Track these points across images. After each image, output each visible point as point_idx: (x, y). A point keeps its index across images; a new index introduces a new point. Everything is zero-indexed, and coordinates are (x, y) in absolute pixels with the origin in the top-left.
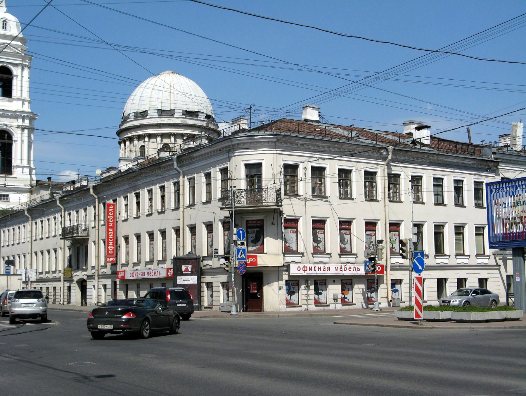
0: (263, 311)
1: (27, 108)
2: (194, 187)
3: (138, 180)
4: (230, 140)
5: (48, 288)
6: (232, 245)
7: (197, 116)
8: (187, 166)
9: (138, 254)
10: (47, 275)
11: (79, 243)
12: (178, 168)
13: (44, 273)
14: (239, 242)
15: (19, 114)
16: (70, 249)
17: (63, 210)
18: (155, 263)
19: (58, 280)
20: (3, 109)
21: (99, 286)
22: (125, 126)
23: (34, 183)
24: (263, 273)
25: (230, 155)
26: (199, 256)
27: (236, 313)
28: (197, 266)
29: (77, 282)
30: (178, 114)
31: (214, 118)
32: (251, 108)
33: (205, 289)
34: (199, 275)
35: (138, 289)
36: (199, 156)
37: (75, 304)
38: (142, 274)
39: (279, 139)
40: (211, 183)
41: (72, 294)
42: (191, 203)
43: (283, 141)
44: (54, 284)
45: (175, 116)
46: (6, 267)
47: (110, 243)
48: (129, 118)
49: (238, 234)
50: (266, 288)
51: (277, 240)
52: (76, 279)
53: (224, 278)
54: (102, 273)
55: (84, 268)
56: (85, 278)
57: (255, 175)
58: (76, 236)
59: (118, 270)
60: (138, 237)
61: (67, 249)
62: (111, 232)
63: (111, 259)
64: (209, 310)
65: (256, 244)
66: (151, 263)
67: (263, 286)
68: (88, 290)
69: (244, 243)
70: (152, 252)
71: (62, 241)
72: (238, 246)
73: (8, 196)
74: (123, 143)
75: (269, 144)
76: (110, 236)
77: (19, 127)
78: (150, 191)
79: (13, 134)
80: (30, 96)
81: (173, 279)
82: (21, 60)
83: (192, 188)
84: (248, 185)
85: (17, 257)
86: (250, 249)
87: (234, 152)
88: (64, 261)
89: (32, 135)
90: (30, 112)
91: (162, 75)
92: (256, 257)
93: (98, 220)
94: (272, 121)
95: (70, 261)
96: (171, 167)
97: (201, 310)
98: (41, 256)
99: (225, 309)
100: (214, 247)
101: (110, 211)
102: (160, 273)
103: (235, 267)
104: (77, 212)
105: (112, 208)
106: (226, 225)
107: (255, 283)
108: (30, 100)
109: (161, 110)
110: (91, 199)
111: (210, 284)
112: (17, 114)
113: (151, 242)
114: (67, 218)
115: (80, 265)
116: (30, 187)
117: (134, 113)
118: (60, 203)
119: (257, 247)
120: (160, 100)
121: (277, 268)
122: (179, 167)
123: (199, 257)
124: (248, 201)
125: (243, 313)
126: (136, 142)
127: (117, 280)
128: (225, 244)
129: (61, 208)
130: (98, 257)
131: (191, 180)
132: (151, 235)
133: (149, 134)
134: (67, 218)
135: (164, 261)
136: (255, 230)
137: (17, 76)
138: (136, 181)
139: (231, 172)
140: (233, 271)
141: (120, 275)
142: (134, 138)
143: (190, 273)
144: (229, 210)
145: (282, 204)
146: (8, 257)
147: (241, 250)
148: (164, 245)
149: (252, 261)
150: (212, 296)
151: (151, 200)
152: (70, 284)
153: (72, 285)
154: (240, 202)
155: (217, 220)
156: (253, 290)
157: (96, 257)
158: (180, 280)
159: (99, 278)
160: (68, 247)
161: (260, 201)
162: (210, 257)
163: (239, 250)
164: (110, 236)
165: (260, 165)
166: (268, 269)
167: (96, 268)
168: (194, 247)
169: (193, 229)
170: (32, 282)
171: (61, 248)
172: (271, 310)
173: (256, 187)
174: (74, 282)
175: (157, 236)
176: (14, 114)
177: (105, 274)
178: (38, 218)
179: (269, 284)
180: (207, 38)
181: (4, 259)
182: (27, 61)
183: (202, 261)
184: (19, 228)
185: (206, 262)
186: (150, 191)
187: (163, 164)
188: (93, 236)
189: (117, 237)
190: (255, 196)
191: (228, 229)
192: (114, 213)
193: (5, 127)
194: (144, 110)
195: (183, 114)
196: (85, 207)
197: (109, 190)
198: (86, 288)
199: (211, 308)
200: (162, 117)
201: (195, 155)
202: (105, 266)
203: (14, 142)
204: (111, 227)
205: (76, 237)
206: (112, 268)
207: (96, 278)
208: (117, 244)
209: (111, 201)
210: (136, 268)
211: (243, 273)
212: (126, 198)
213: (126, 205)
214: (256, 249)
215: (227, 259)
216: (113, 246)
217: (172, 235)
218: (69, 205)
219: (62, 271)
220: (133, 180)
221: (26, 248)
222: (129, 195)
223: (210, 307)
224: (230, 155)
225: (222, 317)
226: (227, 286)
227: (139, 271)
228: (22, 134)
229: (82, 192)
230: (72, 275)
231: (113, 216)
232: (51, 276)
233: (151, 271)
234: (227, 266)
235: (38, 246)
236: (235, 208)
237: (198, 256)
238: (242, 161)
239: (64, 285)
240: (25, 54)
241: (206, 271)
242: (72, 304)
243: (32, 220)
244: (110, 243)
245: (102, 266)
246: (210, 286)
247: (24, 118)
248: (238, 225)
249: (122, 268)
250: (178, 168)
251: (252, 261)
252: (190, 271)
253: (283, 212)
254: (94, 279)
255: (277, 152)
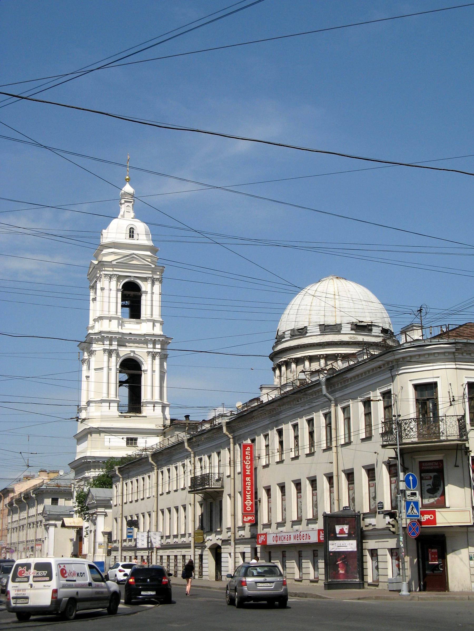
0: (448, 591)
1: (158, 330)
2: (349, 419)
3: (281, 412)
4: (392, 353)
5: (176, 556)
6: (399, 496)
7: (371, 330)
8: (340, 391)
9: (284, 511)
10: (176, 540)
11: (212, 497)
12: (328, 395)
13: (172, 537)
14: (408, 493)
15: (149, 338)
16: (201, 505)
17: (192, 455)
18: (304, 522)
19: (187, 546)
20: (131, 333)
21: (236, 554)
22: (280, 347)
23: (168, 423)
24: (446, 535)
25: (393, 374)
26: (359, 512)
27: (408, 593)
28: (356, 527)
29: (210, 549)
30: (346, 329)
31: (393, 333)
32: (422, 309)
33: (368, 558)
34: (360, 539)
35: (284, 558)
36: (354, 377)
37: (208, 578)
38: (288, 538)
39: (458, 349)
40: (370, 413)
41: (204, 565)
42: (347, 441)
43: (465, 351)
44: (184, 551)
45: (342, 332)
46: (128, 529)
47: (247, 496)
48: (284, 338)
49: (407, 481)
50: (450, 558)
51: (463, 489)
52: (208, 544)
53: (392, 543)
54: (240, 536)
55: (219, 530)
56: (219, 543)
57: (428, 399)
58: (207, 488)
59: (259, 533)
60: (282, 487)
61: (198, 505)
62: (249, 481)
63: (249, 518)
64: (374, 588)
65: (435, 494)
66: (298, 523)
67: (447, 554)
68: (223, 560)
69: (416, 493)
70: (299, 509)
71: (192, 495)
72: (408, 498)
73: (136, 439)
74: (278, 369)
75: (445, 356)
76: (247, 487)
77: (149, 353)
78: (295, 426)
79: (143, 365)
80: (162, 315)
81: (323, 544)
82: (151, 272)
83: (348, 419)
84: (418, 412)
85: (141, 517)
86: (426, 501)
87: (398, 369)
88: (194, 521)
89: (165, 364)
90: (162, 335)
91: (324, 282)
92: (434, 513)
93: (219, 465)
94: (449, 325)
95: (201, 521)
96: (320, 394)
97: (363, 588)
98: (169, 514)
99: (395, 587)
100: (378, 500)
101: (247, 454)
102: (309, 536)
103: (404, 528)
104: (209, 457)
105: (249, 450)
106: (392, 468)
107: (435, 550)
108: (162, 320)
109: (324, 325)
110: (225, 440)
111: (376, 551)
112: (147, 338)
113: (299, 494)
114: (198, 465)
115: (214, 527)
116: (163, 428)
117: (290, 331)
118: (189, 446)
119: (436, 499)
120: (322, 313)
121: (465, 528)
122: (330, 393)
123: (359, 514)
124: (419, 434)
125: (420, 593)
126: (293, 366)
127: (257, 546)
128: (392, 495)
129: (189, 453)
130: (234, 515)
131: (346, 409)
132: (298, 484)
133: (310, 356)
134: (198, 465)
135: (314, 520)
136: (432, 475)
137: (146, 292)
138: (278, 414)
139: (396, 396)
140: (401, 532)
141: (261, 539)
142: (291, 362)
143: (346, 535)
144: (394, 449)
145: (467, 437)
146: (131, 516)
147: (412, 504)
148: (315, 497)
149: (429, 518)
150: (377, 568)
151: (296, 437)
152: (202, 552)
153: (204, 553)
154: (409, 437)
155: (380, 463)
156: (433, 560)
157: (231, 515)
158: (334, 546)
159: (235, 544)
160: (199, 502)
161: (438, 434)
162: (373, 513)
163: (408, 504)
164: (247, 487)
165: (435, 384)
166: (452, 530)
167: (232, 530)
168: (352, 500)
169: (350, 475)
170: (158, 549)
171: (190, 504)
172: (460, 589)
173: (431, 415)
174: (206, 549)
175: (306, 486)
176: (143, 339)
177: (244, 538)
178: (164, 466)
179: (456, 552)
180: (325, 213)
181: (126, 519)
182: (158, 273)
183: (363, 520)
184: (143, 479)
185: (368, 521)
186: (295, 426)
187: (310, 390)
188: (228, 489)
189: (256, 489)
190: (428, 428)
191: (395, 475)
192: (251, 456)
193: (132, 355)
194: (302, 326)
195: (352, 329)
196: (218, 451)
197: (246, 426)
198: (221, 557)
199: (377, 586)
200: (326, 334)
201: (350, 375)
202: (243, 528)
203: (143, 373)
204: (248, 476)
205: (207, 490)
206: (252, 530)
207: (232, 543)
208: (256, 498)
209: (249, 442)
210: (280, 529)
211: (415, 536)
212: (266, 436)
213: (267, 446)
214: (434, 502)
215: (392, 515)
216: (252, 501)
217: (323, 484)
218: (201, 448)
219: (192, 535)
220: (275, 412)
221: (149, 505)
222: (270, 432)
223: (375, 584)
224: (393, 374)
225: (388, 598)
226: (397, 555)
227: (283, 534)
228: (153, 362)
229: (214, 431)
230: (204, 539)
231: (251, 460)
232: (179, 540)
233: (298, 533)
234: (393, 526)
235: (164, 502)
236: (400, 445)
237: (356, 512)
238: (410, 380)
239: (194, 552)
240: (155, 266)
241: (370, 533)
242: (204, 578)
243: (158, 469)
244: (247, 496)
245: (239, 528)
246: (375, 555)
247: (154, 343)
248: (407, 469)
249: (263, 530)
250: (328, 395)
251: (429, 518)
252: (347, 534)
253: (470, 450)
254: (230, 544)
255: (458, 366)
